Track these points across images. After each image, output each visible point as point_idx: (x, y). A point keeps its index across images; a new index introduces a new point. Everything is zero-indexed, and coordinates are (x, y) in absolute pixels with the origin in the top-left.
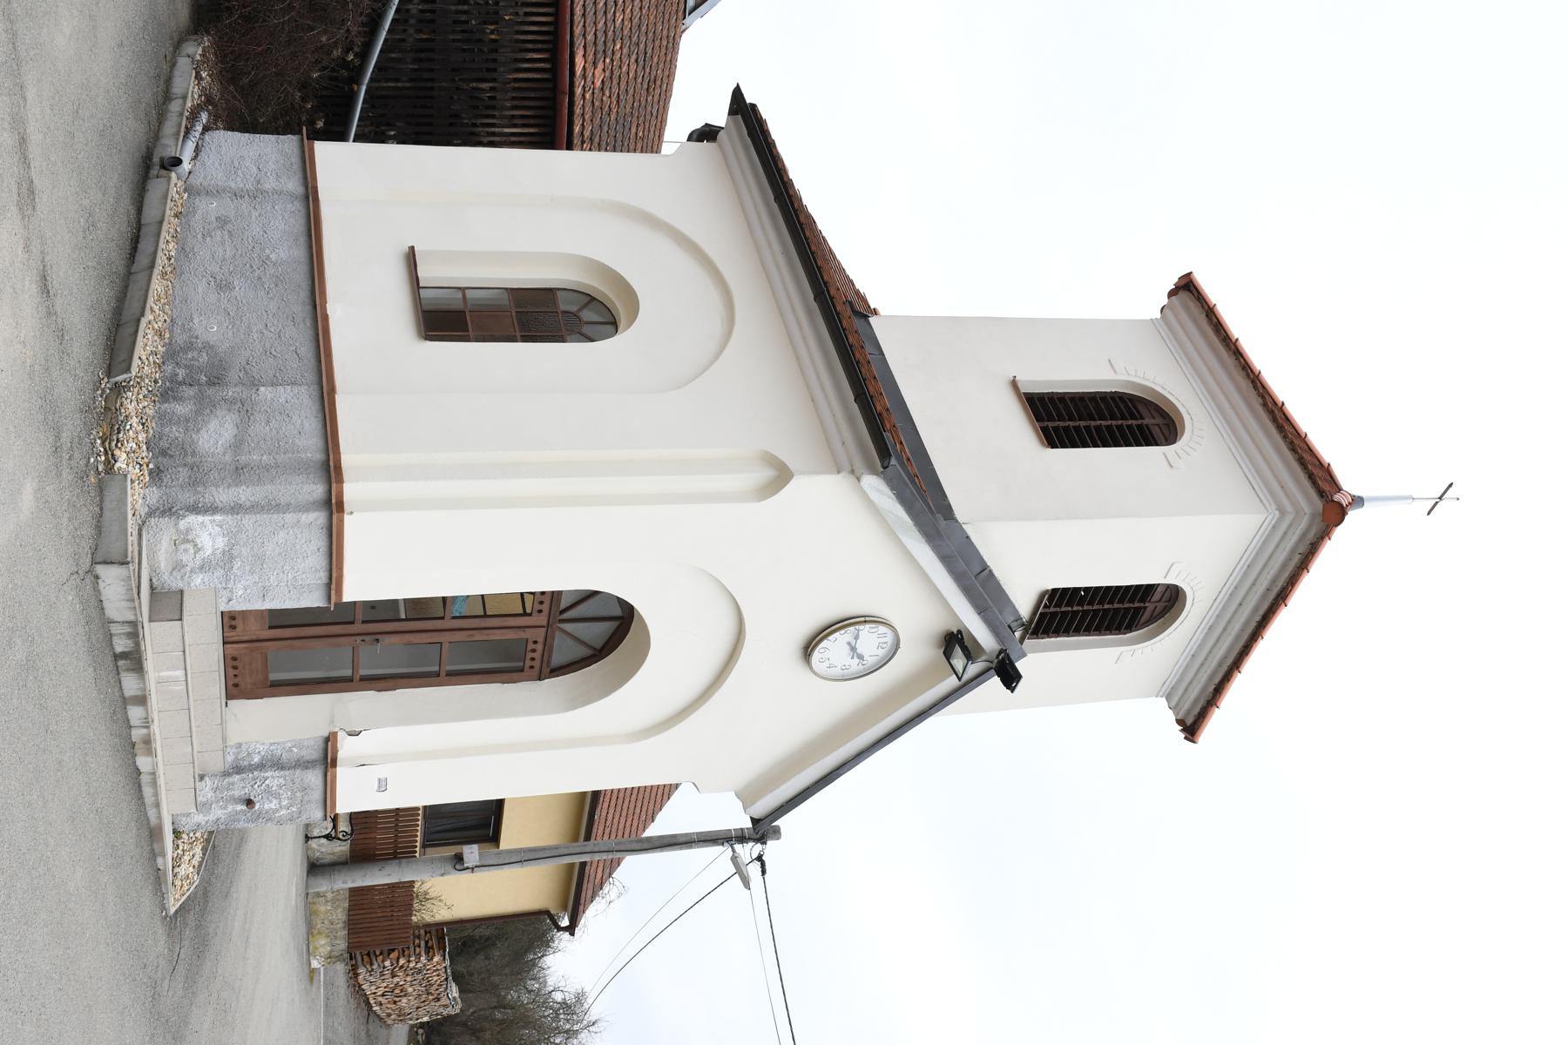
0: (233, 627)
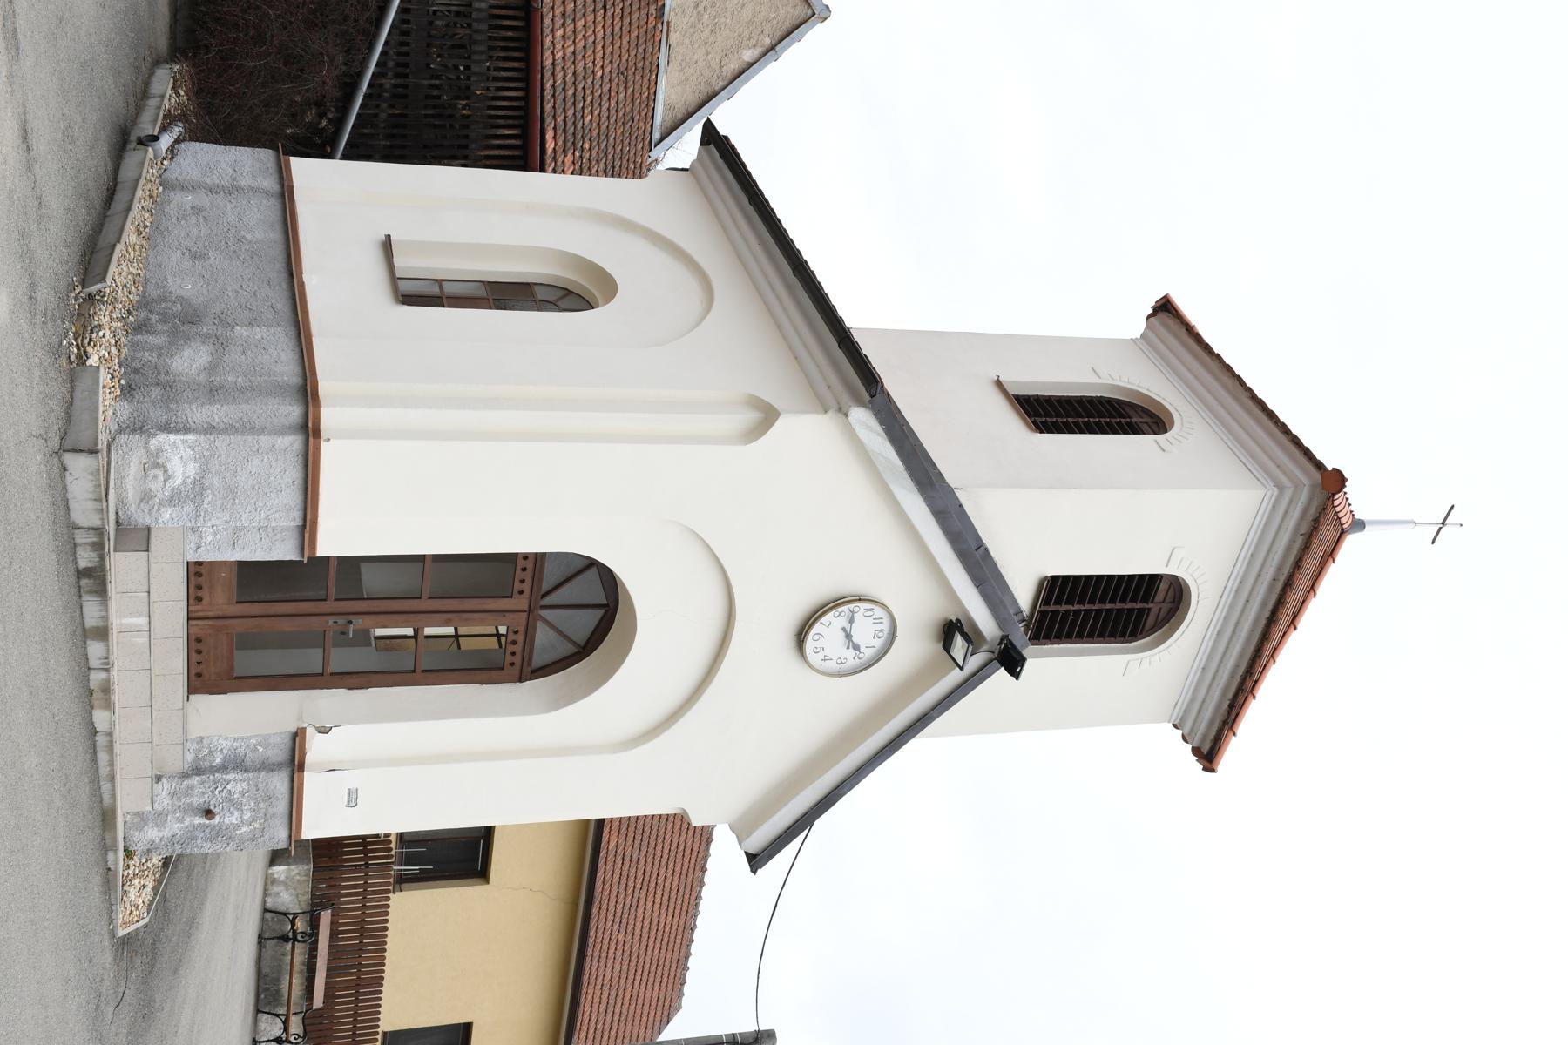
0: (199, 599)
